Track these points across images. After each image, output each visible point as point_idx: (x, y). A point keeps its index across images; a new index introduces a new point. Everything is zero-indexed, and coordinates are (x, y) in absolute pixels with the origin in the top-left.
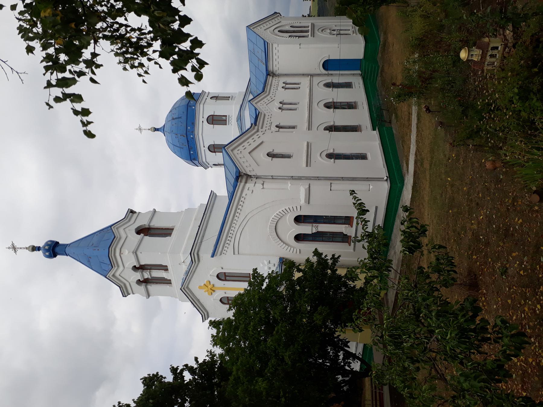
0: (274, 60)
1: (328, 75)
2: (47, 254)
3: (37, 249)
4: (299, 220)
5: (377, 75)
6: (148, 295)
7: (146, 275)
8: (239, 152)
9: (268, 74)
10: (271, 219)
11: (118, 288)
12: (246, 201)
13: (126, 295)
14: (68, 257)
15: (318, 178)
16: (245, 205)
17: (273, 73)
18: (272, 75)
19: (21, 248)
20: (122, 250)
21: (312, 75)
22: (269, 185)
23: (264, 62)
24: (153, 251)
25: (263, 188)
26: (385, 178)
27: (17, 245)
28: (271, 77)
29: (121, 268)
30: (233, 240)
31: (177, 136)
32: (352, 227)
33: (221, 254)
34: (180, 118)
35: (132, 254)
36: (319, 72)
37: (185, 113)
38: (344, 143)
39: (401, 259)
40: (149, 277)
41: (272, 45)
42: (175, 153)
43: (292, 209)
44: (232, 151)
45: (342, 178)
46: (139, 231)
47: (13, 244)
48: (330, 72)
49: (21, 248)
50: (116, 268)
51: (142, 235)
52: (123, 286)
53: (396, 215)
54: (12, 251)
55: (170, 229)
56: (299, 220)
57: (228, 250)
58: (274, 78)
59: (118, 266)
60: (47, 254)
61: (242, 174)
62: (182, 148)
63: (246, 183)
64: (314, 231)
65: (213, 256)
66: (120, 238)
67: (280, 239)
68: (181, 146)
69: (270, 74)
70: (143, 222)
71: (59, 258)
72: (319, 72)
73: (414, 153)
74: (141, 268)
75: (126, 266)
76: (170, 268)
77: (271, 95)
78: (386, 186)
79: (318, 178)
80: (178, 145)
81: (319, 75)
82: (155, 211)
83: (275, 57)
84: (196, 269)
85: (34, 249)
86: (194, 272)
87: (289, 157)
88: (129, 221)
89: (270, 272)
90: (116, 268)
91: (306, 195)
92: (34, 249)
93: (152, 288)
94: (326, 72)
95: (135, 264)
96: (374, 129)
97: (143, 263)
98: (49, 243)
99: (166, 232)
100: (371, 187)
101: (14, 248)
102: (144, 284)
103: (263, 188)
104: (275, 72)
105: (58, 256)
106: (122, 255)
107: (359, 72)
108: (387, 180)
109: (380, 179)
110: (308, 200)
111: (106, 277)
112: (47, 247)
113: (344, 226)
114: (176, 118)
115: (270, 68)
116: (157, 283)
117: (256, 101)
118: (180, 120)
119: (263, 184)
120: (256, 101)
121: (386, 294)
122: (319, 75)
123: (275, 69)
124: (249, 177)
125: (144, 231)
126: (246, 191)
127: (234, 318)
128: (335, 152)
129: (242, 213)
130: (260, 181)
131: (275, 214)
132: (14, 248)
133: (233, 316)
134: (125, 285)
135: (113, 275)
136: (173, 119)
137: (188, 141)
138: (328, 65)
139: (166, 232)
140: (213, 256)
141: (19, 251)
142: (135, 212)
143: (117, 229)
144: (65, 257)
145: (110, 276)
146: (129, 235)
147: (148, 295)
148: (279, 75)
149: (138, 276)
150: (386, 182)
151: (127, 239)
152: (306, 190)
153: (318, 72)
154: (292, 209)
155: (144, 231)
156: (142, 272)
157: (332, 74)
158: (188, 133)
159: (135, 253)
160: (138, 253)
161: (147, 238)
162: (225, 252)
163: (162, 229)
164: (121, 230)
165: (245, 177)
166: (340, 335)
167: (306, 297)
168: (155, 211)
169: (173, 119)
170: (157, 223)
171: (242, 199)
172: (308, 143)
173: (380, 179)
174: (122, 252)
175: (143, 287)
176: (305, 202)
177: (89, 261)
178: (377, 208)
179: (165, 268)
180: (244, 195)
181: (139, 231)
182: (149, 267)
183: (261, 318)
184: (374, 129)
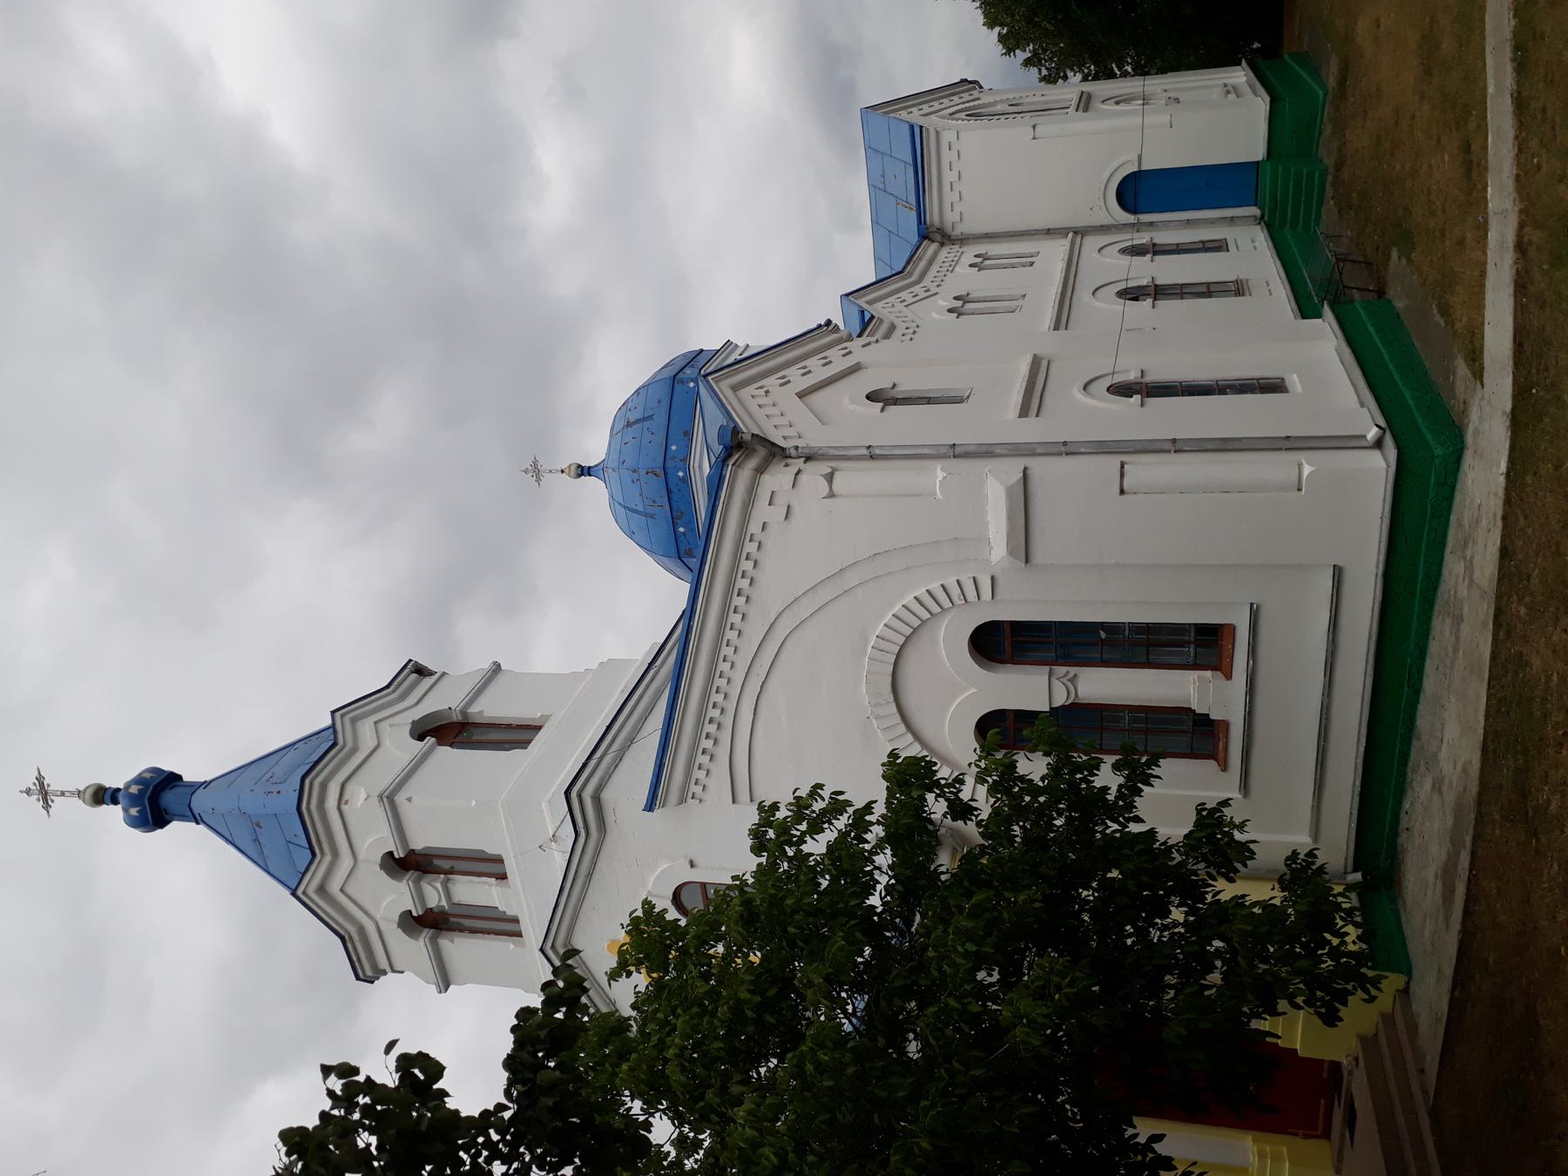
0: (947, 188)
1: (1137, 227)
2: (134, 811)
3: (108, 797)
4: (995, 643)
5: (1320, 204)
6: (445, 982)
7: (434, 896)
8: (762, 392)
9: (925, 235)
10: (873, 641)
11: (338, 941)
12: (767, 559)
13: (369, 973)
14: (202, 827)
15: (1067, 449)
16: (763, 578)
17: (940, 230)
18: (938, 237)
19: (63, 794)
20: (349, 787)
21: (1080, 232)
22: (851, 478)
23: (913, 200)
24: (461, 801)
25: (831, 495)
26: (1372, 433)
27: (53, 784)
28: (934, 246)
29: (346, 862)
30: (725, 736)
31: (636, 476)
32: (1229, 676)
33: (682, 800)
34: (650, 417)
35: (375, 800)
36: (1107, 221)
37: (666, 402)
38: (1181, 342)
39: (1474, 790)
40: (444, 903)
41: (937, 133)
42: (631, 535)
43: (955, 591)
44: (735, 388)
45: (1174, 441)
46: (423, 730)
47: (40, 779)
48: (1145, 218)
49: (63, 794)
50: (328, 859)
51: (430, 740)
52: (356, 937)
53: (1431, 605)
54: (35, 803)
55: (528, 727)
56: (995, 643)
57: (712, 783)
58: (945, 250)
59: (335, 854)
60: (134, 811)
61: (748, 437)
62: (652, 517)
63: (760, 470)
64: (1060, 699)
65: (650, 807)
66: (355, 750)
67: (909, 728)
68: (650, 510)
69: (931, 234)
70: (443, 700)
71: (177, 830)
72: (1105, 220)
73: (1510, 238)
74: (409, 863)
75: (362, 855)
76: (511, 867)
77: (926, 282)
78: (1378, 467)
79: (1067, 449)
80: (640, 508)
81: (1103, 229)
82: (497, 668)
83: (949, 177)
84: (594, 864)
85: (102, 796)
86: (590, 876)
87: (957, 400)
88: (403, 697)
89: (803, 793)
90: (328, 859)
91: (1011, 519)
92: (102, 796)
93: (458, 948)
94: (1131, 218)
95: (393, 848)
96: (1306, 310)
97: (419, 843)
98: (148, 775)
99: (517, 735)
100: (1307, 470)
101: (43, 793)
102: (427, 933)
103: (831, 495)
104: (948, 229)
105: (175, 826)
106: (344, 807)
107: (1254, 211)
108: (1378, 444)
109: (1350, 443)
110: (1024, 545)
111: (294, 894)
112: (134, 789)
113: (1193, 675)
114: (637, 421)
115: (933, 217)
116: (473, 931)
117: (868, 298)
118: (647, 424)
119: (830, 478)
120: (868, 298)
121: (1405, 992)
122: (1103, 229)
123: (951, 217)
124: (776, 453)
125: (449, 731)
126: (762, 512)
127: (634, 1013)
128: (1147, 379)
129: (752, 611)
130: (817, 470)
131: (888, 618)
132: (43, 793)
133: (634, 1007)
134: (362, 930)
135: (322, 890)
136: (629, 424)
137: (669, 491)
138: (1138, 192)
139: (517, 735)
140: (650, 807)
141: (58, 803)
142: (431, 673)
143: (354, 721)
144: (190, 826)
145: (311, 891)
146: (387, 743)
147: (445, 982)
148: (963, 240)
149: (396, 897)
150: (1376, 454)
151: (379, 752)
152: (1010, 492)
153: (1102, 218)
154: (955, 591)
155: (449, 731)
156: (417, 882)
157: (1151, 224)
158: (669, 464)
159: (389, 799)
160: (400, 799)
161: (445, 752)
162: (698, 789)
163: (509, 727)
164: (366, 728)
165: (762, 452)
166: (1158, 1138)
167: (974, 915)
168: (497, 668)
169: (629, 424)
170: (490, 708)
171: (750, 547)
172: (1036, 363)
173: (1350, 443)
174: (346, 797)
175: (421, 942)
176: (1011, 552)
177: (256, 840)
178: (1338, 574)
179: (491, 866)
180: (754, 528)
181: (423, 730)
182: (445, 864)
183: (737, 1008)
184: (1306, 310)
